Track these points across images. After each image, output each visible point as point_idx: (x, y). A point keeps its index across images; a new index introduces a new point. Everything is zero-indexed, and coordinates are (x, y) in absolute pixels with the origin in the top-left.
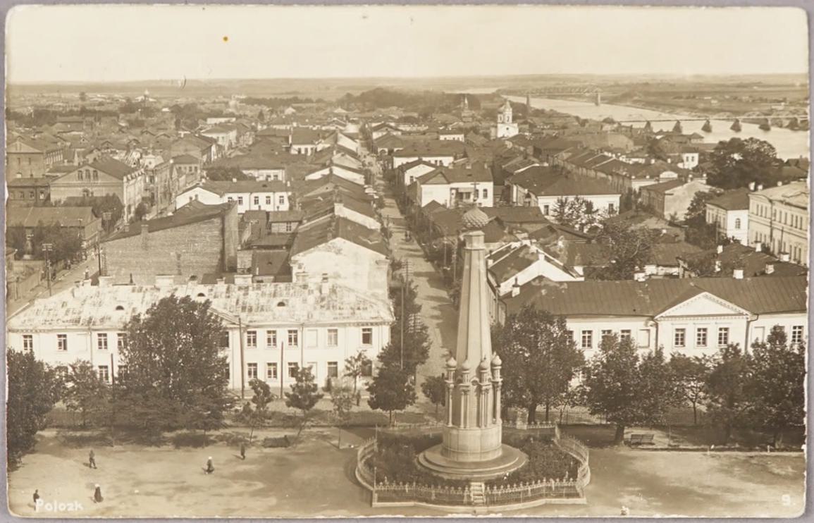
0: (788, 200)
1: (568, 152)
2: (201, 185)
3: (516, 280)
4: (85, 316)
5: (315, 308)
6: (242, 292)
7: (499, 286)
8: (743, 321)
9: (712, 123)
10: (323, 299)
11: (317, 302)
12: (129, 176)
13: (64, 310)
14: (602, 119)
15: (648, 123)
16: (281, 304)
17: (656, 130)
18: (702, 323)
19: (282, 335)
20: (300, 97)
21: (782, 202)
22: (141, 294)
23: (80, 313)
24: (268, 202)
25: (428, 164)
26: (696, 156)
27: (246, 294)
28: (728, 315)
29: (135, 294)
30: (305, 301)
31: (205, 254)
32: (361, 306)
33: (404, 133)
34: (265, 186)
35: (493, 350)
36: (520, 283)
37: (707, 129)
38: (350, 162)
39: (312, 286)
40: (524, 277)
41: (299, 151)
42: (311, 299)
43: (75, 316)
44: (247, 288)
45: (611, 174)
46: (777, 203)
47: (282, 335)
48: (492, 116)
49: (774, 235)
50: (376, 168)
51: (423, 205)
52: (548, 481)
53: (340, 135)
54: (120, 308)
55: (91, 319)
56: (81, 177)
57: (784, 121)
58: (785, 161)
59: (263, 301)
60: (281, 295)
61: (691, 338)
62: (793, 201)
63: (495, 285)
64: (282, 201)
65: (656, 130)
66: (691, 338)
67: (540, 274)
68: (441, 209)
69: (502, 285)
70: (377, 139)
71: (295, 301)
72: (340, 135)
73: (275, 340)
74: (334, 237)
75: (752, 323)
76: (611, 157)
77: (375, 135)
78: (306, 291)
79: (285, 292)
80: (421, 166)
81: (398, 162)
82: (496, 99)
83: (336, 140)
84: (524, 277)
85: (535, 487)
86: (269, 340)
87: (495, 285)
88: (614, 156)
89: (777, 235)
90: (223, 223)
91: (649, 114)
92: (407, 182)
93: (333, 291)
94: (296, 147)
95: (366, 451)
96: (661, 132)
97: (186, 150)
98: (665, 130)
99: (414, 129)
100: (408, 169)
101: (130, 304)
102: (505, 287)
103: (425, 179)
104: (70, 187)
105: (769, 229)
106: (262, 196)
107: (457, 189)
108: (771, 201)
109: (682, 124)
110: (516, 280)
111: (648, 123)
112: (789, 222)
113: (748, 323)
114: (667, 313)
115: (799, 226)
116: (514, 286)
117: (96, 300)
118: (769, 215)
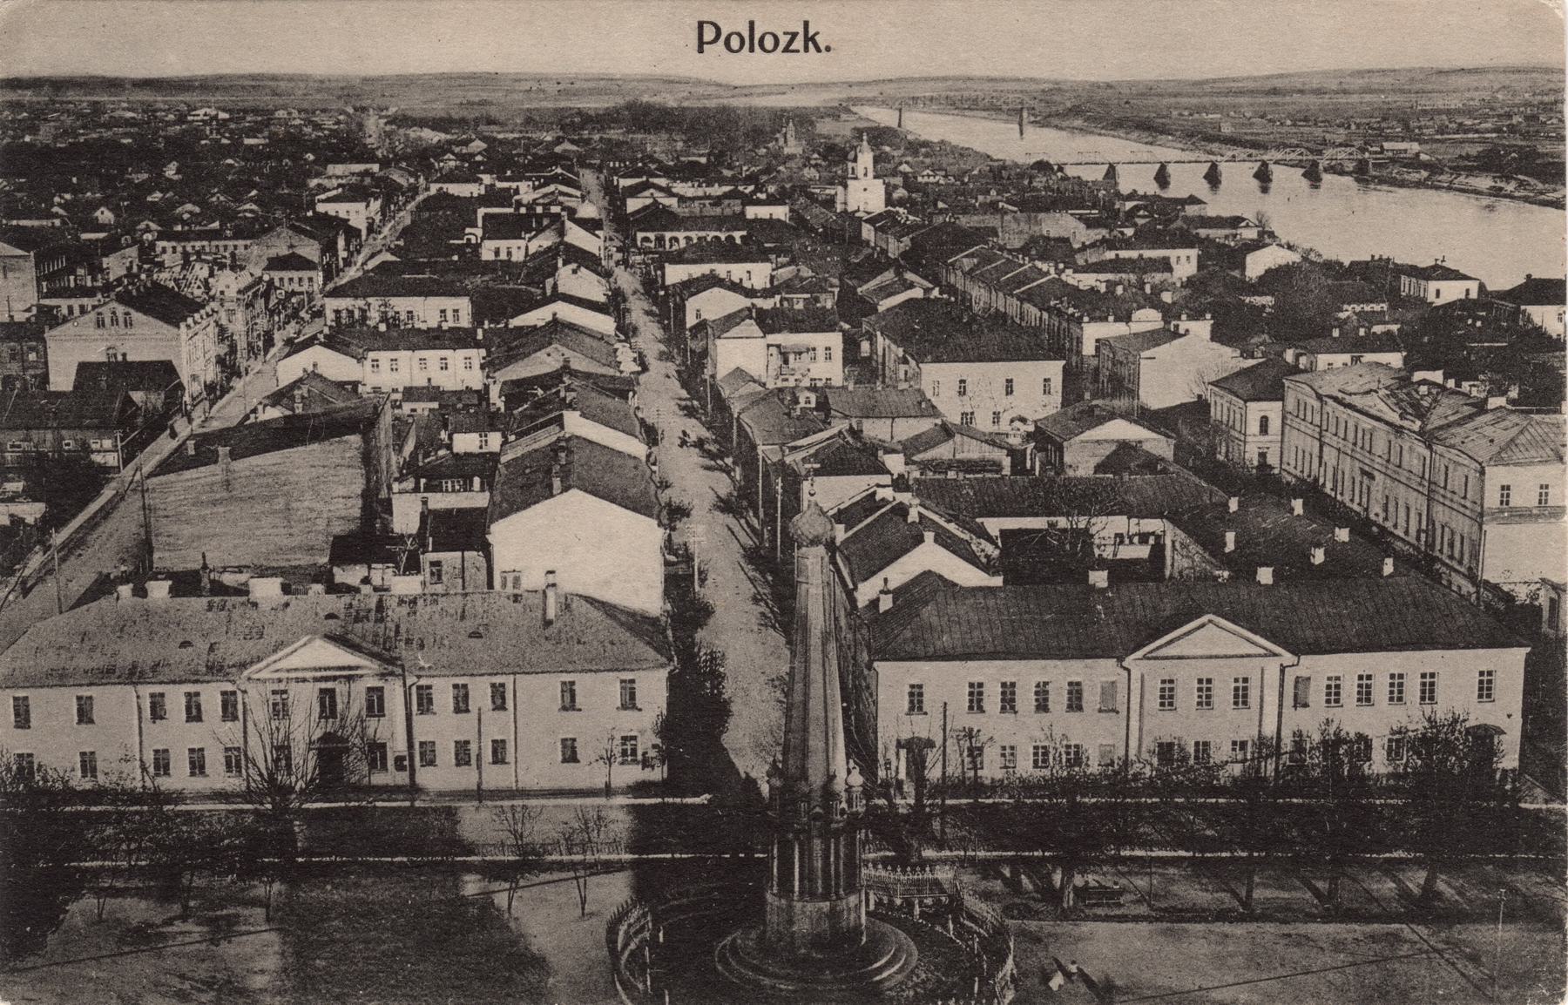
0: (1348, 399)
1: (972, 255)
2: (321, 337)
3: (886, 580)
6: (405, 609)
7: (856, 588)
8: (1272, 667)
9: (1224, 168)
12: (197, 316)
14: (1033, 161)
15: (1111, 172)
16: (475, 635)
17: (1125, 187)
20: (494, 112)
21: (1335, 399)
26: (1194, 253)
28: (1249, 656)
33: (682, 199)
34: (437, 338)
36: (892, 586)
37: (1213, 178)
40: (900, 572)
45: (1048, 310)
46: (1330, 401)
49: (1325, 458)
53: (568, 224)
55: (134, 666)
56: (100, 324)
57: (1346, 163)
58: (1347, 264)
61: (1187, 696)
62: (1357, 401)
63: (851, 586)
66: (1187, 696)
69: (860, 586)
70: (633, 214)
72: (568, 224)
76: (1048, 273)
77: (633, 205)
80: (716, 291)
81: (675, 274)
82: (844, 116)
83: (561, 232)
84: (900, 572)
87: (851, 586)
88: (1052, 270)
89: (1330, 456)
90: (366, 441)
95: (632, 930)
97: (291, 246)
98: (1141, 193)
102: (866, 592)
104: (97, 525)
105: (1317, 444)
107: (778, 346)
108: (1319, 397)
110: (886, 580)
111: (1111, 172)
112: (1351, 436)
115: (1367, 447)
116: (882, 592)
118: (1317, 420)
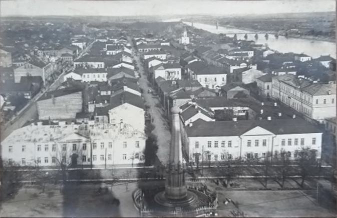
3: (191, 120)
4: (33, 138)
5: (118, 134)
8: (271, 137)
9: (259, 35)
10: (121, 130)
11: (119, 131)
13: (25, 135)
15: (235, 35)
16: (106, 132)
17: (238, 39)
18: (257, 138)
19: (106, 145)
21: (283, 82)
22: (54, 129)
23: (31, 137)
24: (99, 77)
25: (159, 59)
26: (253, 52)
27: (93, 128)
29: (52, 129)
30: (114, 131)
31: (76, 105)
32: (135, 133)
33: (148, 42)
35: (183, 157)
36: (193, 121)
38: (129, 60)
39: (117, 125)
40: (194, 118)
41: (110, 53)
42: (117, 130)
43: (29, 138)
44: (93, 126)
47: (106, 145)
48: (179, 32)
50: (137, 58)
51: (156, 78)
52: (204, 207)
54: (46, 135)
59: (99, 131)
60: (106, 128)
62: (286, 82)
64: (104, 77)
65: (238, 39)
67: (199, 118)
68: (163, 80)
71: (111, 131)
73: (103, 146)
74: (124, 103)
75: (274, 138)
78: (115, 127)
79: (107, 127)
81: (146, 57)
83: (123, 49)
84: (194, 118)
85: (199, 210)
86: (101, 146)
89: (282, 93)
91: (236, 31)
92: (150, 66)
93: (125, 126)
94: (108, 51)
96: (240, 40)
99: (151, 40)
100: (150, 61)
101: (50, 133)
102: (187, 123)
103: (157, 67)
106: (96, 74)
107: (168, 71)
109: (248, 35)
111: (235, 35)
113: (273, 138)
114: (245, 134)
117: (37, 131)
